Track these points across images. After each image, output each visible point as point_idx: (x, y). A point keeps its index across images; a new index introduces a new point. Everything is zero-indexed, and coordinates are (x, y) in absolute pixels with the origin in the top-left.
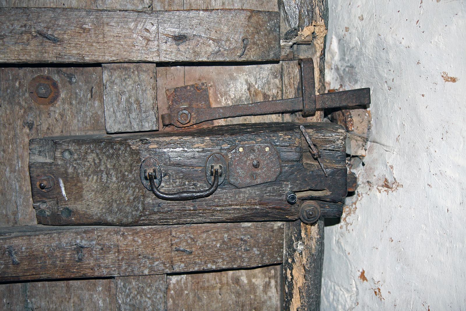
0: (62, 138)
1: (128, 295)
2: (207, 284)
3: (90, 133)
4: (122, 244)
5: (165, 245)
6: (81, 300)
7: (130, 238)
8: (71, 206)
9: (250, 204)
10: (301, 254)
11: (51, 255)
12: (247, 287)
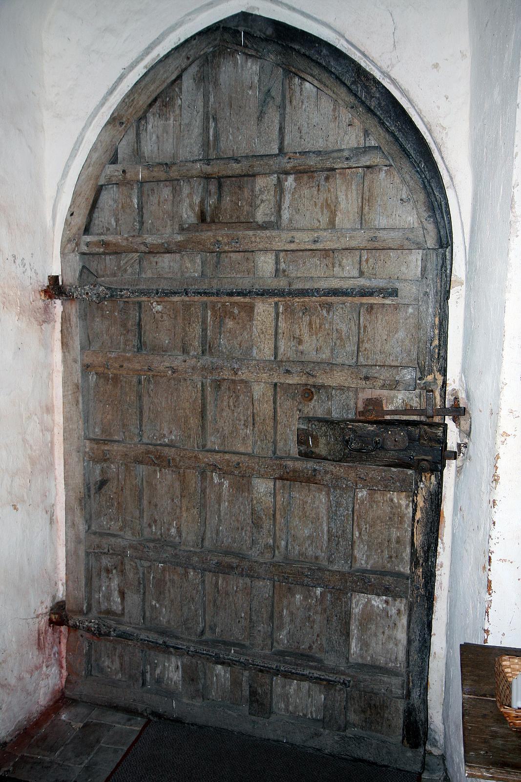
0: (312, 418)
1: (335, 497)
2: (376, 500)
3: (325, 416)
4: (334, 471)
5: (354, 474)
6: (314, 497)
7: (338, 468)
8: (313, 450)
9: (393, 459)
10: (422, 489)
11: (302, 471)
12: (397, 505)
